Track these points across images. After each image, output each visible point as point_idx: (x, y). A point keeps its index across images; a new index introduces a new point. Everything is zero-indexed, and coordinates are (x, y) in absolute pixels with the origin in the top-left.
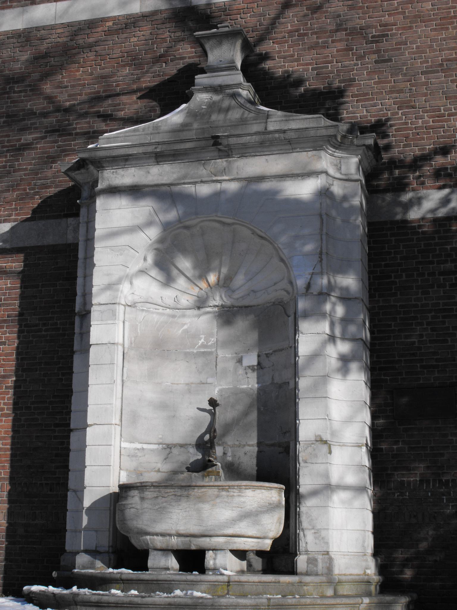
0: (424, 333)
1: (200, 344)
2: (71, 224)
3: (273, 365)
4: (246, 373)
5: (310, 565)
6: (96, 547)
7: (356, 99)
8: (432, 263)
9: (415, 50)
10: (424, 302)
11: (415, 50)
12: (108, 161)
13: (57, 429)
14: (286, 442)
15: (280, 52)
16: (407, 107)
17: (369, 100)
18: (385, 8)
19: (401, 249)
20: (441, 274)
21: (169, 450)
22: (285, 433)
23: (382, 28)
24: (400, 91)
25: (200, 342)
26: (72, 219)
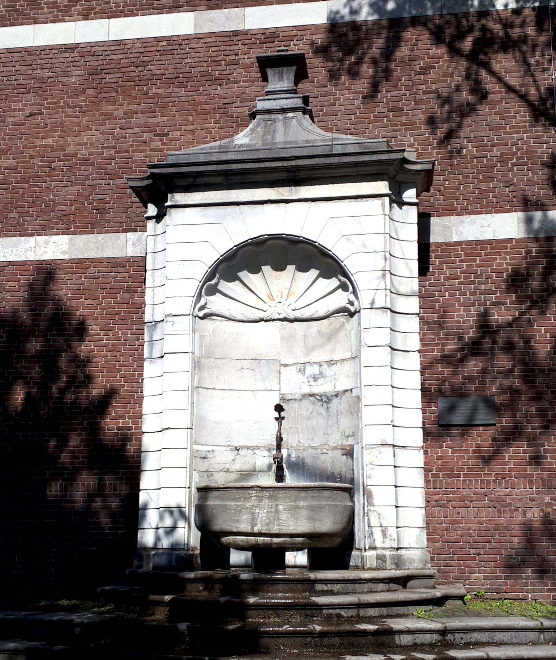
2: (130, 238)
3: (335, 374)
4: (308, 382)
19: (445, 270)
21: (237, 452)
23: (429, 60)
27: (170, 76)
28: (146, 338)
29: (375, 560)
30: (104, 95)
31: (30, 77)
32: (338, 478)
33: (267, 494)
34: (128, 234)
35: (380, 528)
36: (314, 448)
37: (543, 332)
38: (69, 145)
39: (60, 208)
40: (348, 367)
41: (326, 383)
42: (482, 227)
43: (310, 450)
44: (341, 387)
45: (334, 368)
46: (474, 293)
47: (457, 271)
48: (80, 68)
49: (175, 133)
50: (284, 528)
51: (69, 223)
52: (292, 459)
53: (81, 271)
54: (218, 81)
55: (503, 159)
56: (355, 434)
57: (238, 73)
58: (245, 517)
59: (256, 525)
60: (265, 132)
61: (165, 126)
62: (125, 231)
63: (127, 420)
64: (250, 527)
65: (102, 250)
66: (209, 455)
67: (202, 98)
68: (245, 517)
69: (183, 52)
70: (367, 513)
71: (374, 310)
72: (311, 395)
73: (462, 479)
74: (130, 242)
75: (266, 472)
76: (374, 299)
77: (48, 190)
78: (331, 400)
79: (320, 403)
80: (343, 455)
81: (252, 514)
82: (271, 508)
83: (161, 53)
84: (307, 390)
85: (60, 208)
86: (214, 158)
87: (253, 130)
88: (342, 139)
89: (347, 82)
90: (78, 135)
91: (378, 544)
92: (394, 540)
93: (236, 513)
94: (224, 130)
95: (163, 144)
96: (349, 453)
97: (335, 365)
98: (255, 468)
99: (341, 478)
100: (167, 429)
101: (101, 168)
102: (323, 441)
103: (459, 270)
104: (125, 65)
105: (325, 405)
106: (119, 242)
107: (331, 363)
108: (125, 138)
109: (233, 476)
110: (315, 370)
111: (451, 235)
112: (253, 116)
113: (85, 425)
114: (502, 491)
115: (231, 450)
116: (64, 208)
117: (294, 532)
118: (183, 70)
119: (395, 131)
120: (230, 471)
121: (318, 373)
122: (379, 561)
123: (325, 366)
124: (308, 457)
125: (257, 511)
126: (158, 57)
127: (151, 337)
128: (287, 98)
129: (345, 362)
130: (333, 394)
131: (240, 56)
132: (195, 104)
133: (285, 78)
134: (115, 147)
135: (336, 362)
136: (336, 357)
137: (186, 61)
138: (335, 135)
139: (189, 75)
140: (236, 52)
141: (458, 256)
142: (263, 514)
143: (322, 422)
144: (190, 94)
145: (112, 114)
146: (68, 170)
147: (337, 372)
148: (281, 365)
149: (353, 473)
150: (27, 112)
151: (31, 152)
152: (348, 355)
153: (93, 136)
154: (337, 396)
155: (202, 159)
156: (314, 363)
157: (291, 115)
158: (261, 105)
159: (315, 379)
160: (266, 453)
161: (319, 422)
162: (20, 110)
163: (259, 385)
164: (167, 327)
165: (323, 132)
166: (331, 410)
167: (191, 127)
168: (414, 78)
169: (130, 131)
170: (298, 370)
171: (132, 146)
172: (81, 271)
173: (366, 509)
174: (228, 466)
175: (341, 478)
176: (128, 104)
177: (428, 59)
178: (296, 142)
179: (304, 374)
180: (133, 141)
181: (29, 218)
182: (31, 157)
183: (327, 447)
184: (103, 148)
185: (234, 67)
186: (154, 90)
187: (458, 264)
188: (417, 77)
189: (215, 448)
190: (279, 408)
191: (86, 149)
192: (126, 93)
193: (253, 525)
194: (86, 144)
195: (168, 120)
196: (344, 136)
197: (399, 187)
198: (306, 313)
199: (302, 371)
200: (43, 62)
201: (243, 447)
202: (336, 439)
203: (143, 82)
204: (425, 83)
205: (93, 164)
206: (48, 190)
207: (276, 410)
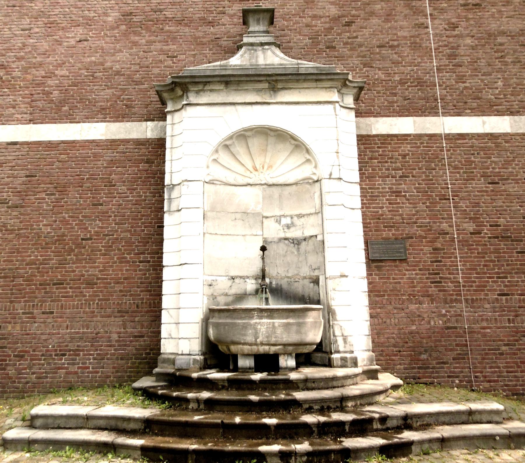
0: (384, 206)
4: (283, 229)
6: (190, 352)
8: (387, 162)
10: (383, 186)
13: (141, 264)
14: (316, 276)
15: (287, 27)
16: (368, 67)
17: (344, 60)
18: (353, 6)
20: (393, 170)
24: (364, 56)
26: (150, 122)
28: (166, 196)
29: (340, 360)
30: (132, 29)
31: (80, 16)
34: (148, 122)
36: (288, 277)
37: (434, 196)
38: (107, 62)
39: (100, 104)
40: (313, 220)
41: (296, 230)
42: (391, 125)
43: (286, 280)
44: (307, 234)
45: (302, 220)
46: (388, 169)
48: (116, 11)
49: (182, 56)
50: (280, 340)
51: (106, 114)
53: (114, 147)
54: (211, 24)
55: (402, 82)
56: (322, 267)
57: (225, 19)
59: (258, 338)
60: (250, 57)
61: (175, 51)
62: (146, 120)
64: (254, 339)
65: (129, 134)
66: (214, 283)
67: (201, 34)
68: (250, 331)
69: (187, 4)
71: (332, 180)
72: (286, 239)
74: (149, 128)
75: (254, 295)
76: (331, 173)
77: (91, 91)
78: (301, 243)
79: (292, 245)
80: (311, 283)
81: (256, 329)
82: (270, 324)
83: (172, 4)
84: (282, 235)
85: (100, 104)
86: (217, 73)
87: (242, 56)
88: (305, 64)
90: (113, 55)
91: (341, 349)
94: (215, 55)
95: (174, 63)
96: (316, 281)
98: (246, 292)
99: (309, 299)
100: (184, 264)
101: (129, 77)
102: (296, 272)
104: (147, 11)
105: (296, 246)
106: (141, 128)
107: (300, 216)
108: (147, 58)
109: (230, 299)
110: (288, 221)
111: (371, 130)
112: (239, 47)
113: (115, 259)
114: (413, 307)
115: (229, 279)
116: (102, 104)
117: (286, 343)
118: (187, 16)
119: (331, 61)
122: (343, 361)
123: (295, 218)
124: (284, 284)
126: (170, 7)
127: (170, 195)
128: (263, 36)
130: (302, 238)
131: (226, 9)
132: (196, 38)
133: (261, 23)
134: (139, 64)
135: (304, 216)
136: (304, 212)
137: (189, 10)
138: (300, 61)
140: (224, 5)
141: (377, 144)
143: (295, 259)
144: (192, 31)
145: (137, 42)
146: (106, 78)
147: (304, 223)
148: (263, 217)
149: (319, 296)
150: (78, 39)
151: (79, 65)
152: (313, 211)
153: (124, 56)
154: (305, 240)
155: (208, 73)
156: (287, 216)
157: (266, 47)
158: (246, 40)
159: (288, 227)
160: (254, 281)
161: (291, 258)
162: (72, 37)
163: (248, 232)
164: (184, 188)
165: (290, 59)
166: (300, 250)
167: (193, 53)
169: (150, 54)
171: (151, 63)
172: (114, 147)
173: (331, 323)
174: (227, 291)
175: (309, 299)
176: (150, 36)
178: (273, 65)
179: (280, 223)
180: (152, 60)
181: (77, 111)
182: (80, 69)
183: (298, 277)
184: (131, 64)
185: (223, 15)
189: (218, 278)
190: (263, 249)
191: (119, 64)
192: (148, 29)
194: (119, 61)
195: (177, 48)
196: (306, 62)
198: (281, 181)
199: (279, 222)
200: (89, 6)
201: (237, 277)
202: (305, 271)
203: (160, 22)
204: (349, 32)
205: (124, 75)
206: (91, 91)
207: (261, 250)
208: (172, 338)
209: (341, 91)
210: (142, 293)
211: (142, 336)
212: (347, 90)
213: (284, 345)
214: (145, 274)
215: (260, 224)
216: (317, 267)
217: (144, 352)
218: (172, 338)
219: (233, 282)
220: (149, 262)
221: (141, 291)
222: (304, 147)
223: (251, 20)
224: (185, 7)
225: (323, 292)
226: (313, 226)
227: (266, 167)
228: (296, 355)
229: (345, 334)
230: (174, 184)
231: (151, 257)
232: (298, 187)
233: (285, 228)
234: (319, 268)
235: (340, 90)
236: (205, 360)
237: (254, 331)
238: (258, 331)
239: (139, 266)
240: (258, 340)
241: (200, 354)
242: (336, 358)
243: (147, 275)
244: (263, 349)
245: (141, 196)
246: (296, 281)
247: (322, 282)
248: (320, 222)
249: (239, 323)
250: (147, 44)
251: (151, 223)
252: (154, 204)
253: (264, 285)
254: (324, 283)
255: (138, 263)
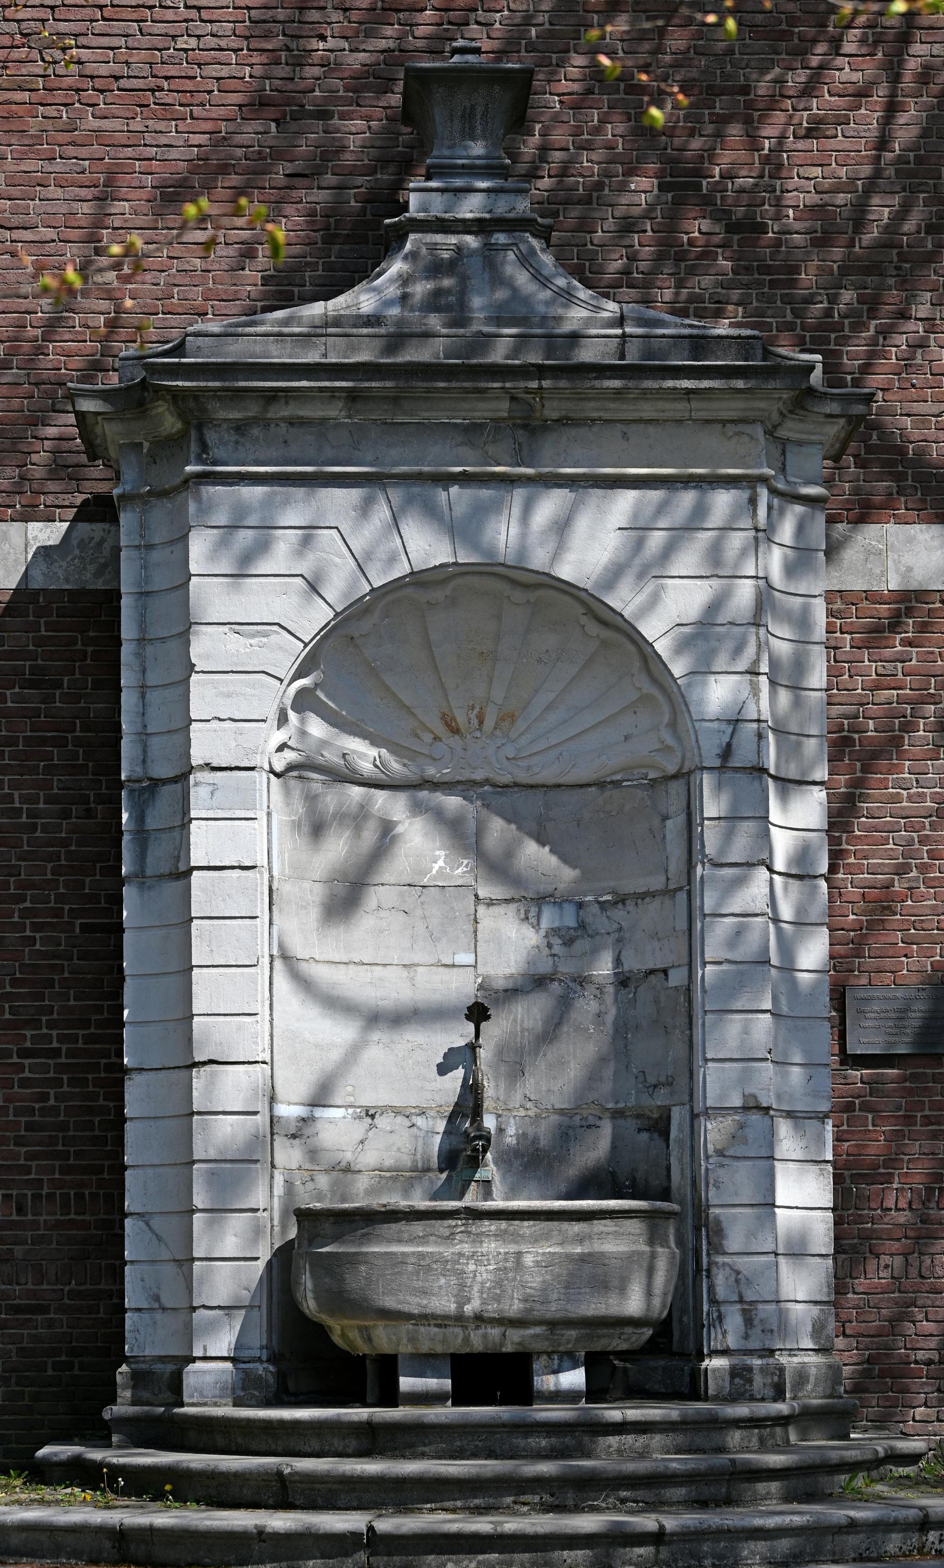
1: (434, 872)
3: (620, 929)
5: (737, 1380)
7: (768, 278)
9: (912, 165)
11: (912, 165)
12: (220, 398)
13: (27, 1062)
21: (369, 1120)
22: (655, 1086)
23: (833, 99)
25: (436, 867)
27: (135, 83)
32: (627, 1187)
33: (493, 1228)
34: (31, 525)
35: (738, 1306)
47: (896, 667)
50: (537, 1306)
52: (509, 1140)
58: (442, 1281)
59: (469, 1300)
62: (25, 518)
63: (45, 1031)
64: (453, 1306)
69: (170, 15)
70: (708, 1271)
73: (895, 1186)
80: (640, 1130)
82: (506, 1260)
89: (621, 140)
92: (772, 1331)
93: (418, 1273)
96: (659, 1126)
97: (620, 906)
103: (900, 665)
111: (884, 573)
118: (172, 71)
120: (353, 1168)
121: (576, 925)
125: (472, 1267)
129: (647, 900)
133: (479, 131)
139: (188, 85)
142: (484, 1276)
152: (657, 882)
168: (794, 147)
169: (27, 235)
170: (523, 916)
174: (349, 1156)
177: (830, 95)
186: (92, 123)
187: (899, 648)
188: (801, 145)
193: (463, 1300)
197: (784, 453)
208: (164, 1309)
209: (782, 433)
210: (34, 1164)
211: (43, 1310)
212: (801, 426)
213: (553, 1324)
214: (44, 1097)
215: (469, 927)
216: (663, 1079)
217: (50, 1361)
218: (164, 1309)
219: (372, 1126)
220: (56, 1053)
221: (31, 1156)
222: (632, 648)
223: (438, 114)
224: (160, 28)
225: (680, 1160)
226: (655, 936)
227: (489, 723)
228: (588, 1354)
229: (750, 1296)
230: (155, 776)
231: (62, 1039)
232: (607, 794)
233: (556, 941)
234: (669, 1083)
235: (775, 427)
236: (281, 1377)
237: (454, 1281)
238: (469, 1282)
239: (20, 1068)
240: (468, 1309)
241: (264, 1358)
242: (715, 1370)
243: (52, 1102)
244: (478, 1340)
245: (18, 812)
246: (589, 1127)
247: (681, 1130)
248: (682, 925)
249: (404, 1254)
250: (15, 191)
251: (58, 913)
252: (65, 843)
253: (480, 1138)
254: (687, 1129)
255: (15, 1060)
